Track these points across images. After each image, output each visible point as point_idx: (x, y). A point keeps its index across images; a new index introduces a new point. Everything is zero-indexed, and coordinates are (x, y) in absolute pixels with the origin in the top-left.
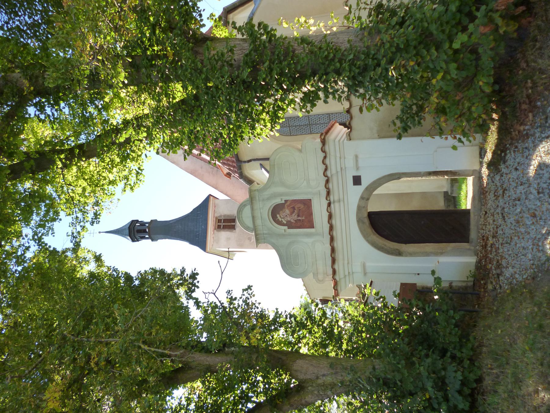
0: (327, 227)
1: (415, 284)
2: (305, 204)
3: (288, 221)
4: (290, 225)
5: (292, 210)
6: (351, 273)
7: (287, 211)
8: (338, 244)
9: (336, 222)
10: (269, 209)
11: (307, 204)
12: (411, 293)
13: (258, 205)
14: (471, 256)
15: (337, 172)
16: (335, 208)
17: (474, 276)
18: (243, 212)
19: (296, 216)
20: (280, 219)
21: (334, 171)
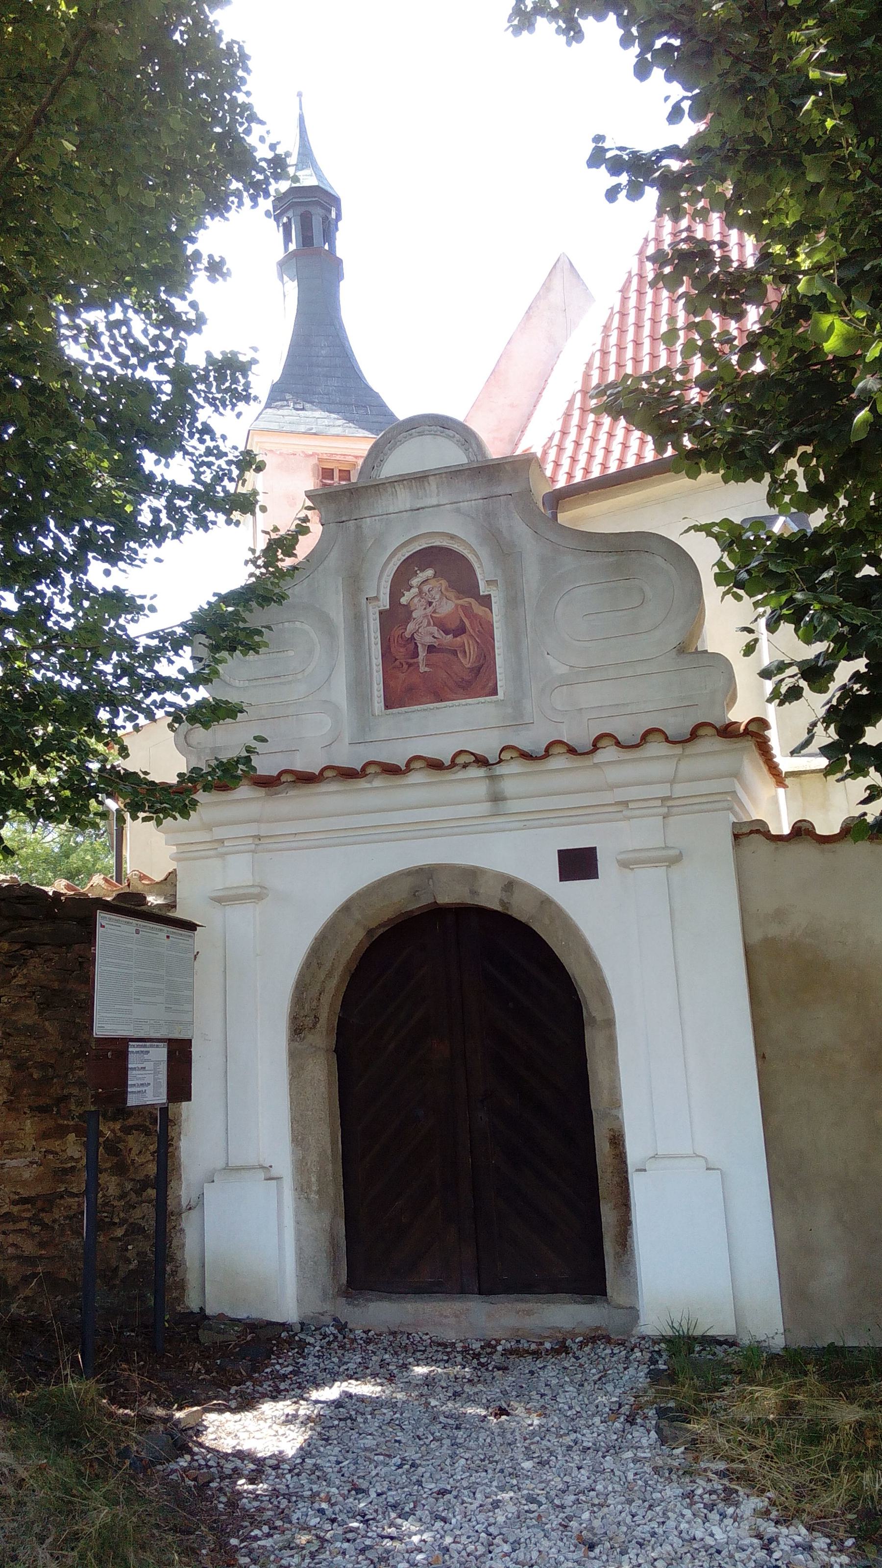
0: (398, 756)
1: (189, 1099)
2: (477, 671)
3: (408, 610)
4: (394, 618)
5: (453, 625)
6: (221, 850)
7: (446, 607)
8: (331, 798)
9: (418, 787)
10: (452, 537)
11: (478, 680)
13: (471, 497)
14: (299, 1301)
15: (611, 787)
16: (472, 784)
18: (441, 441)
19: (429, 640)
20: (415, 582)
21: (613, 774)
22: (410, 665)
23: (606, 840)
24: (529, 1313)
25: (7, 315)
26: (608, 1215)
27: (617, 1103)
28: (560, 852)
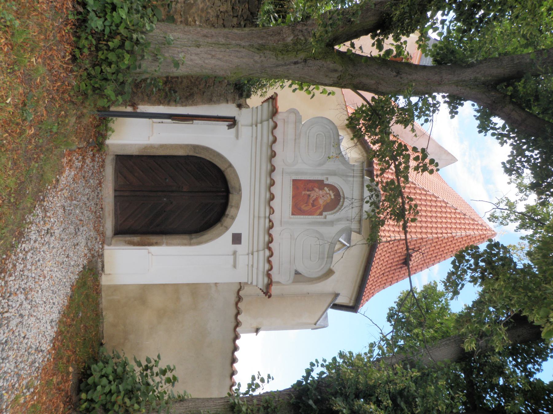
3: (321, 189)
4: (320, 184)
7: (321, 201)
11: (297, 210)
14: (112, 144)
17: (107, 129)
19: (312, 195)
20: (331, 192)
22: (305, 188)
23: (241, 249)
24: (109, 215)
25: (240, 411)
26: (136, 239)
27: (168, 244)
28: (241, 234)
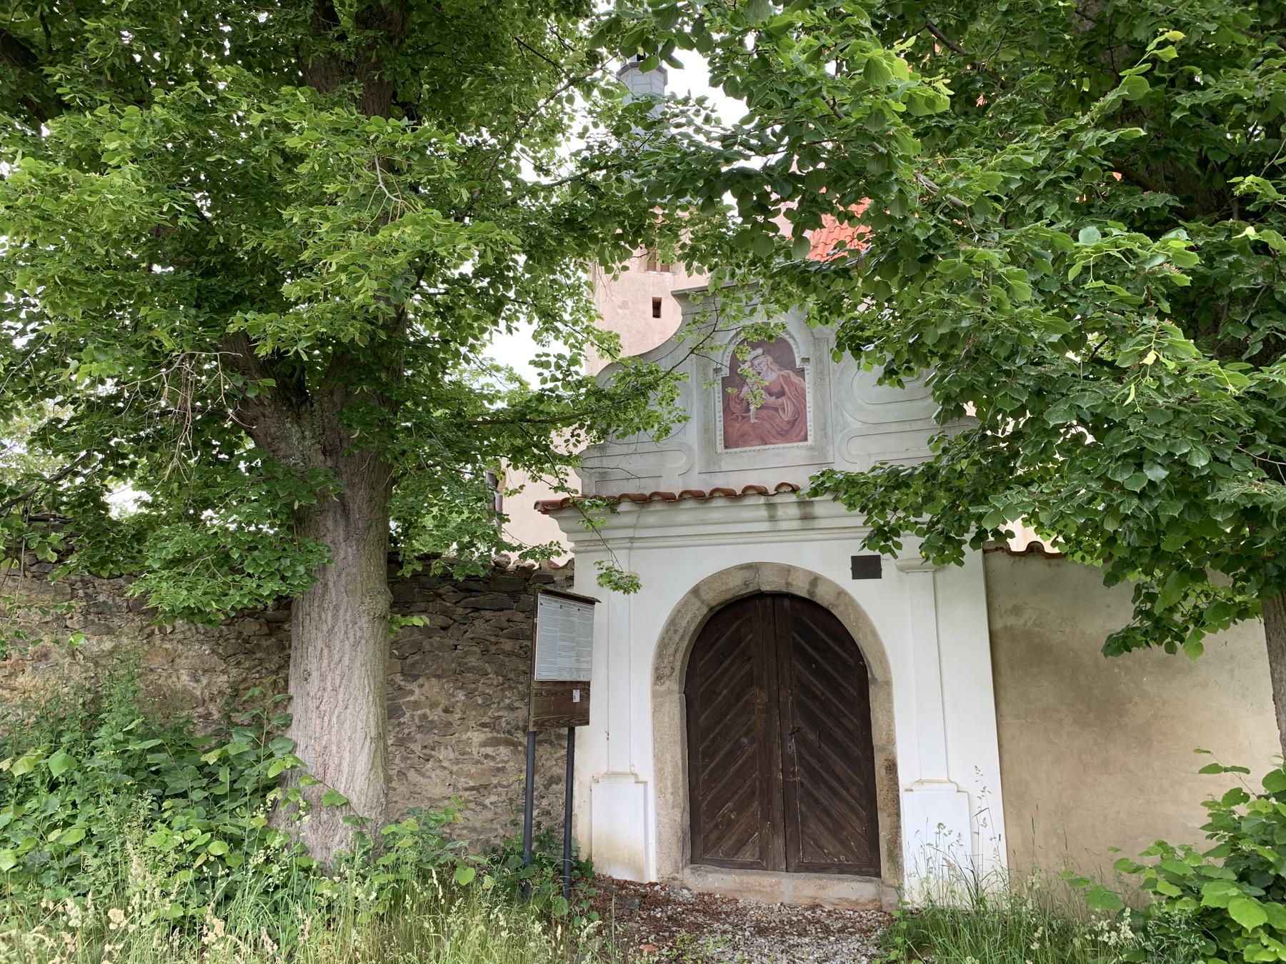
2: (793, 423)
4: (734, 379)
5: (776, 389)
8: (688, 512)
11: (793, 430)
12: (142, 515)
